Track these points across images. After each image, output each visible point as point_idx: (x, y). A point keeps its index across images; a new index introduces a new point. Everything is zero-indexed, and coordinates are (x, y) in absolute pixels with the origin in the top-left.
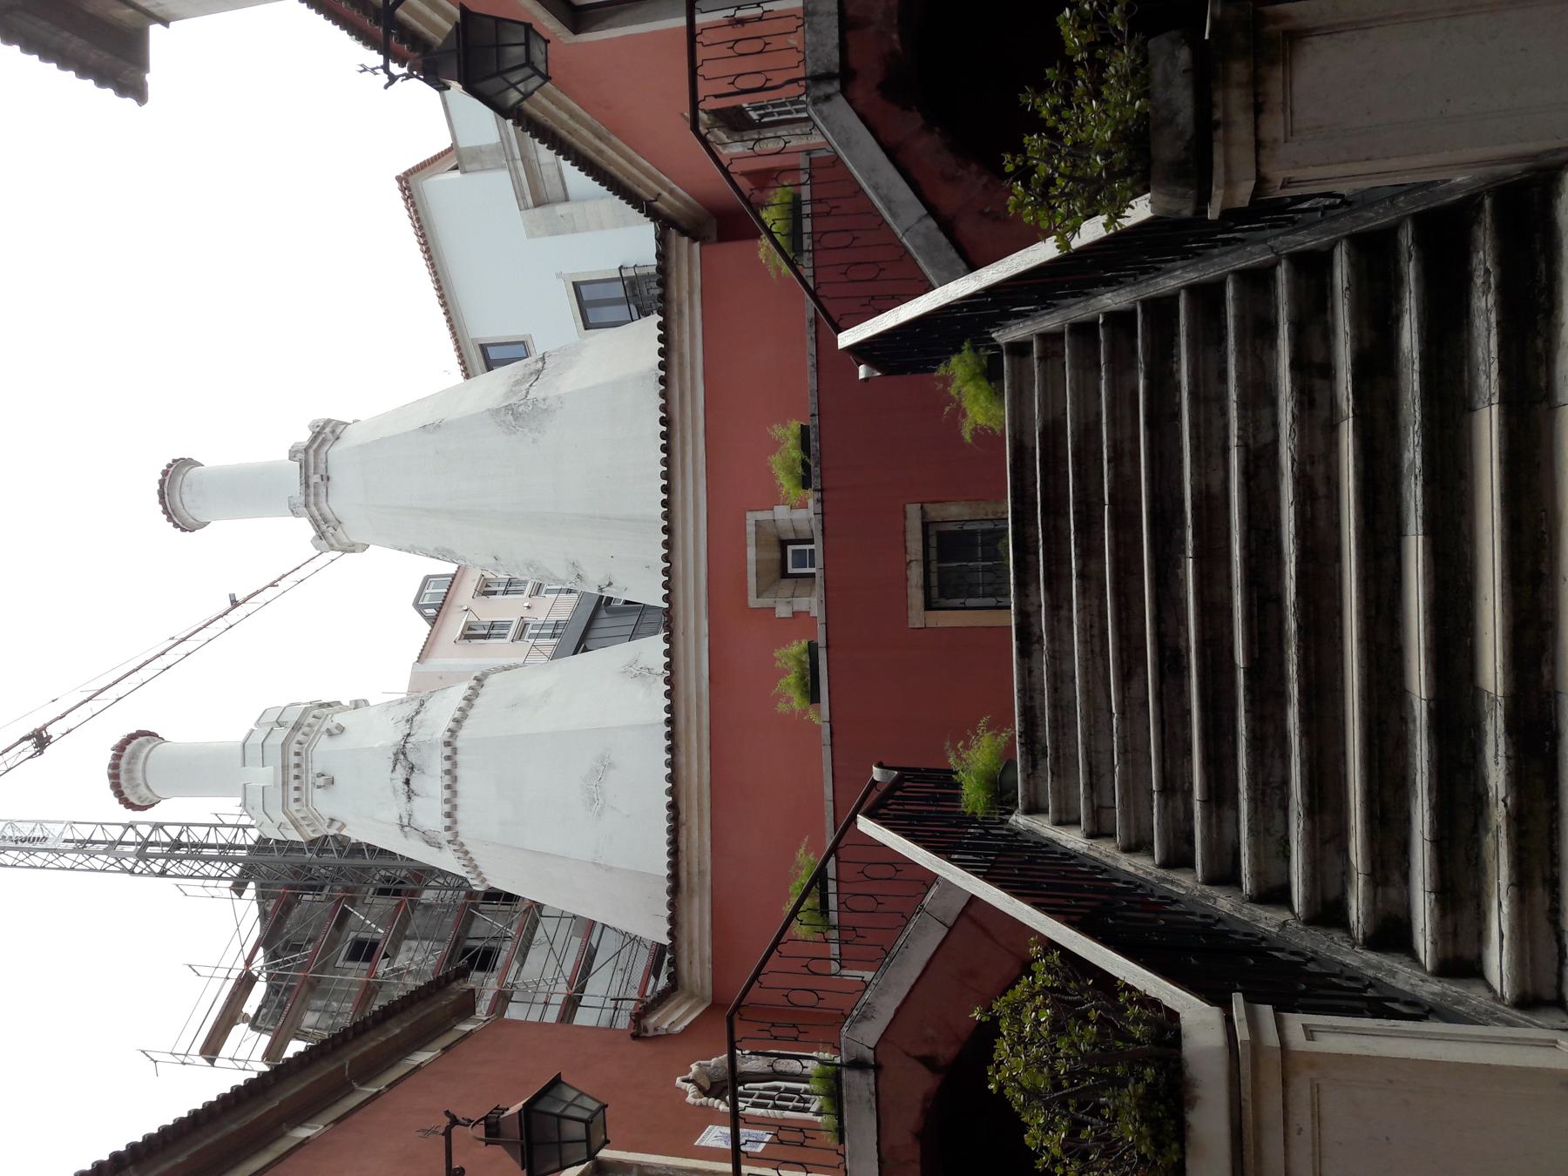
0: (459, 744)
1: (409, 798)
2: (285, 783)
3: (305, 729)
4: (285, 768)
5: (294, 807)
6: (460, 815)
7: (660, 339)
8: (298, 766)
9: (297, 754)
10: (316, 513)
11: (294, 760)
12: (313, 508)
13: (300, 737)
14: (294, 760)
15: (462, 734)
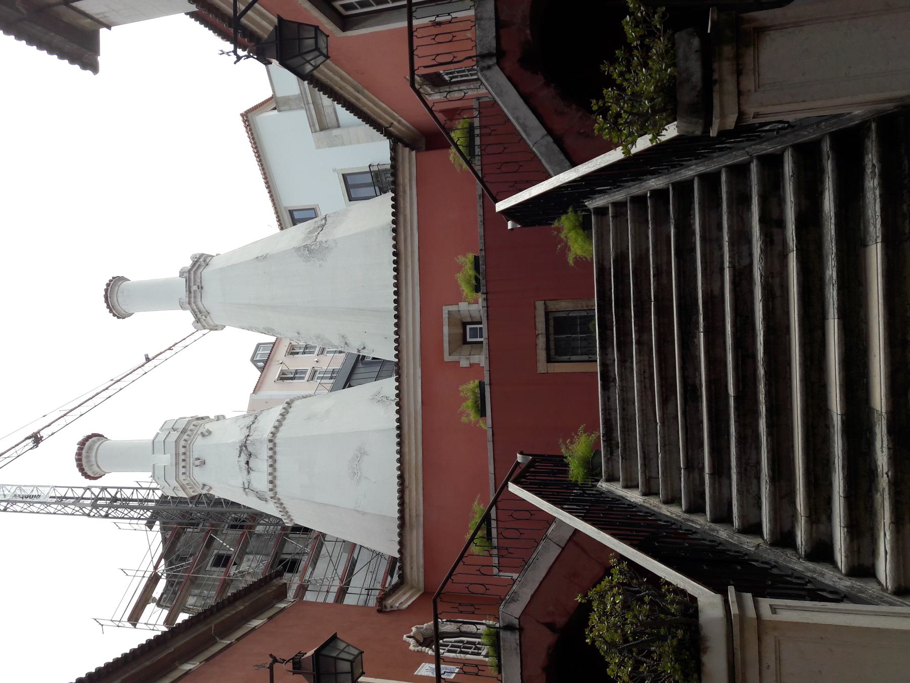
0: (277, 441)
1: (249, 472)
2: (177, 464)
3: (189, 432)
4: (177, 455)
5: (182, 477)
8: (184, 454)
9: (184, 447)
10: (195, 308)
11: (182, 450)
12: (193, 305)
13: (185, 437)
14: (182, 450)
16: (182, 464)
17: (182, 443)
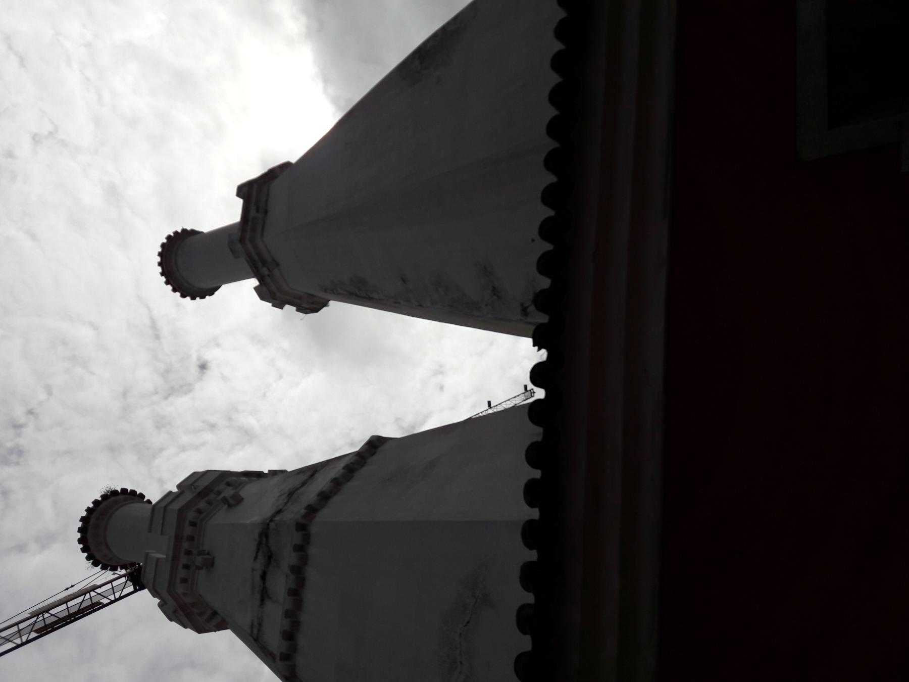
0: (314, 529)
1: (262, 600)
2: (175, 558)
3: (212, 496)
4: (178, 538)
5: (180, 589)
6: (302, 641)
7: (83, 550)
8: (191, 538)
9: (193, 524)
10: (252, 251)
11: (188, 530)
12: (249, 246)
13: (202, 505)
14: (188, 530)
15: (324, 515)
16: (184, 560)
17: (191, 515)
